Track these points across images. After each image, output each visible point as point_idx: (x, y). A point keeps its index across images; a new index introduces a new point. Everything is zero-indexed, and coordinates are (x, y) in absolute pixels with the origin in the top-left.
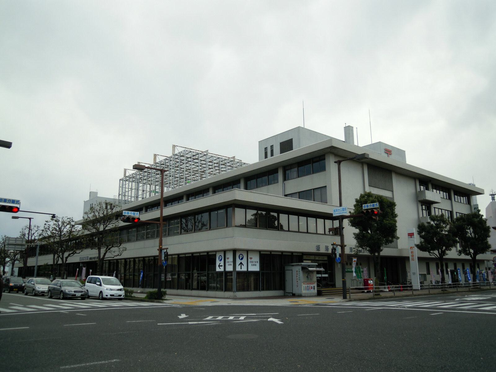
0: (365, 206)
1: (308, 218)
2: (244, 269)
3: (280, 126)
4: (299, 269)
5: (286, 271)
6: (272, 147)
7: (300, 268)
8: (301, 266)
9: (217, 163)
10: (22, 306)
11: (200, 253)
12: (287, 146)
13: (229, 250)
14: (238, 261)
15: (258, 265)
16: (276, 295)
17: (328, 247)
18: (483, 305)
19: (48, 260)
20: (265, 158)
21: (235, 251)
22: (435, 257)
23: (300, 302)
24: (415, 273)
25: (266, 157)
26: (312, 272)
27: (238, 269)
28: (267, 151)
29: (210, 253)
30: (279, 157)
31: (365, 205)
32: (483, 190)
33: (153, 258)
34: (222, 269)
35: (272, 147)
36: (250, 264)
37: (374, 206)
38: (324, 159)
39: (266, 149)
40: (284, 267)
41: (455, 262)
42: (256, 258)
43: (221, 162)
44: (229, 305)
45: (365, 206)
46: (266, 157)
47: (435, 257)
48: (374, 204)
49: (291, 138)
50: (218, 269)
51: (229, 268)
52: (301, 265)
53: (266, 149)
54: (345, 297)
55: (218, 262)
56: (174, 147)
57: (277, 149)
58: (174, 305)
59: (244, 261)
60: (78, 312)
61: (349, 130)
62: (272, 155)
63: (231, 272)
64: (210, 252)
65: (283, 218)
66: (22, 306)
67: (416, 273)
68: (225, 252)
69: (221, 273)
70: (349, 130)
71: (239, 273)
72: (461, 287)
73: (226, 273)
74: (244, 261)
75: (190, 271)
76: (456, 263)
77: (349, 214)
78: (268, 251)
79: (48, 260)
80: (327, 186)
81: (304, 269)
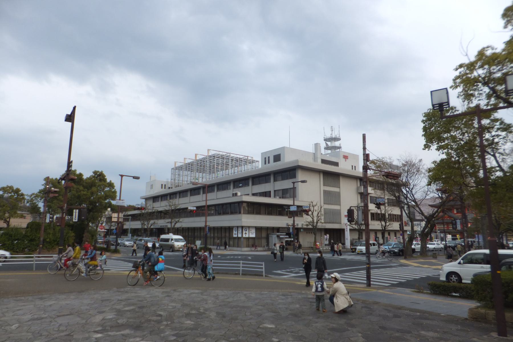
2: (247, 236)
6: (269, 157)
10: (508, 260)
12: (277, 158)
13: (240, 226)
14: (244, 232)
15: (254, 234)
19: (137, 225)
21: (242, 227)
25: (265, 164)
26: (282, 238)
27: (244, 236)
28: (266, 160)
34: (236, 236)
35: (269, 157)
36: (250, 234)
39: (265, 158)
42: (254, 231)
43: (239, 161)
46: (265, 164)
50: (234, 236)
51: (240, 236)
54: (294, 252)
55: (234, 232)
56: (209, 150)
57: (272, 159)
58: (63, 296)
59: (247, 232)
62: (269, 163)
63: (240, 238)
66: (508, 260)
68: (238, 227)
69: (235, 238)
71: (244, 238)
73: (239, 238)
74: (247, 232)
77: (498, 111)
79: (137, 225)
81: (278, 236)
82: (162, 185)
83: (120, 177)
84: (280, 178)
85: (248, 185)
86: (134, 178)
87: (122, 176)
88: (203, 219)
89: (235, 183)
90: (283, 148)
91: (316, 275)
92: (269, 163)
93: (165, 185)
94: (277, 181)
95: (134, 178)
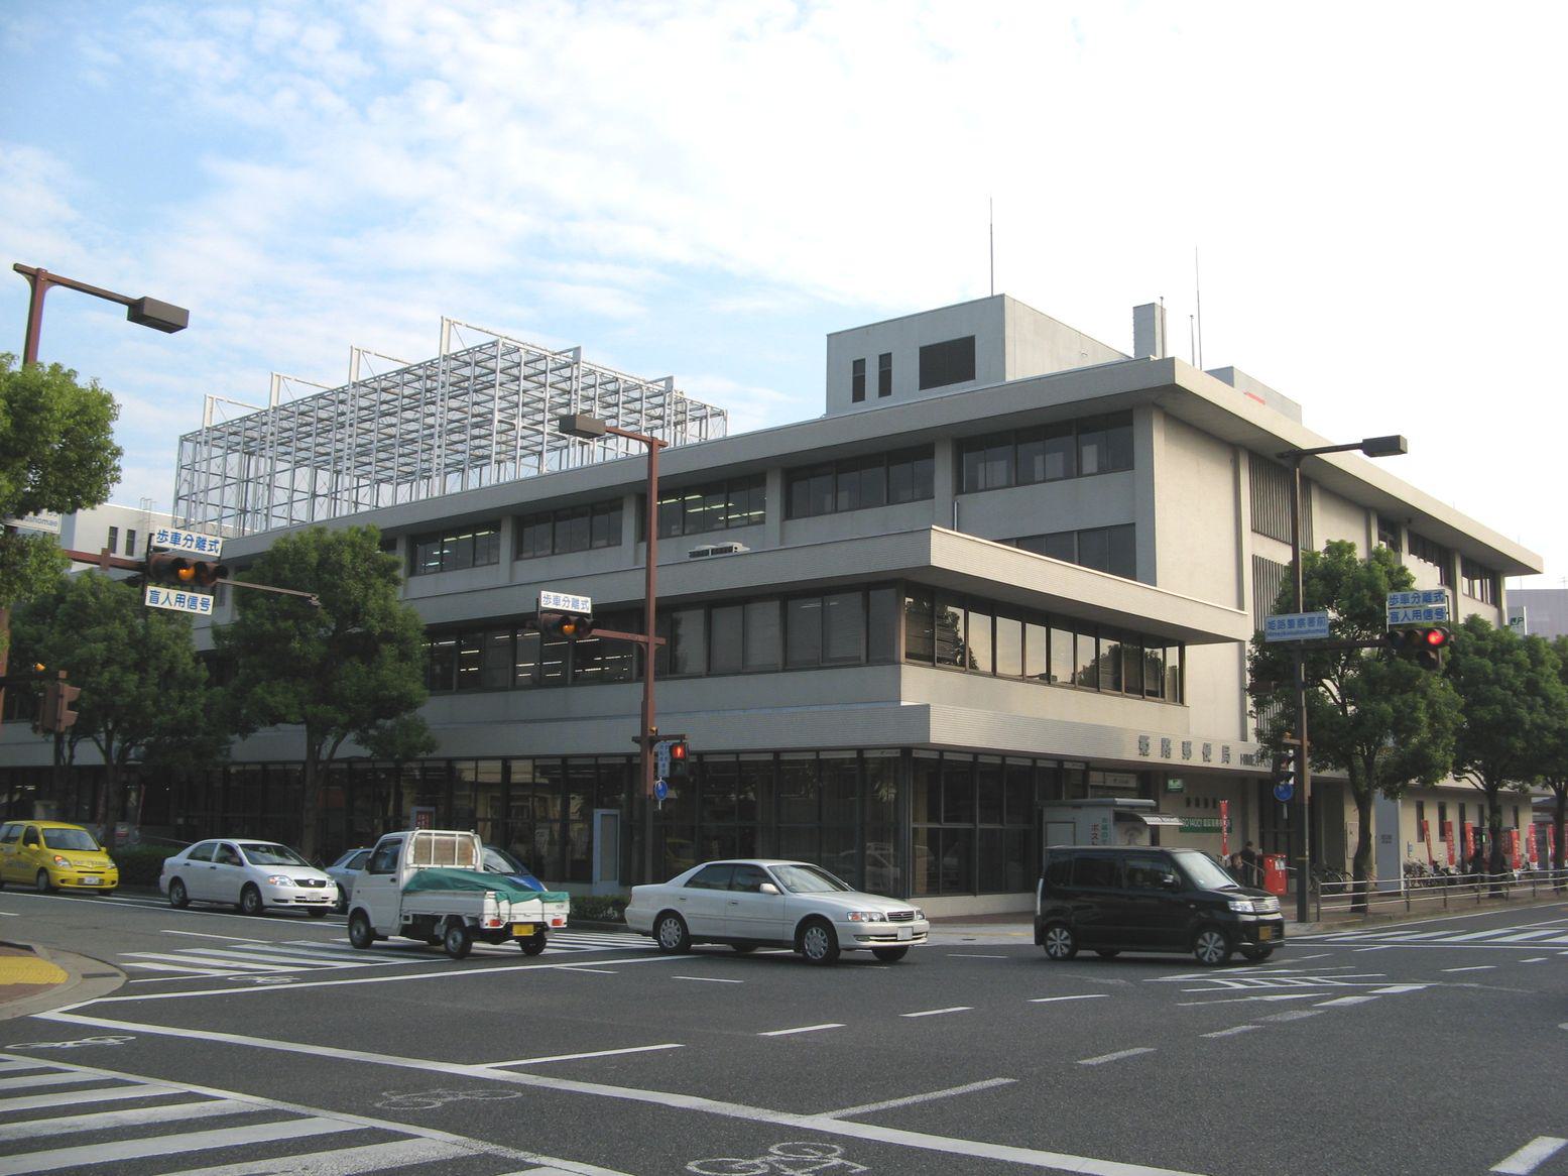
0: (548, 598)
1: (1053, 631)
3: (915, 285)
4: (1104, 820)
5: (1049, 825)
6: (885, 360)
7: (1109, 814)
8: (1112, 809)
9: (458, 409)
11: (737, 753)
16: (1011, 909)
17: (1169, 742)
18: (995, 942)
20: (855, 400)
22: (1474, 787)
23: (390, 937)
24: (1390, 837)
25: (859, 394)
29: (785, 757)
30: (913, 407)
31: (549, 593)
32: (1540, 560)
33: (345, 766)
35: (885, 360)
37: (556, 598)
38: (1130, 423)
39: (859, 366)
40: (1042, 811)
41: (1480, 803)
44: (966, 943)
45: (548, 598)
46: (859, 394)
47: (1474, 787)
48: (195, 599)
49: (965, 334)
52: (1115, 805)
53: (859, 366)
57: (906, 371)
60: (1349, 972)
61: (1146, 319)
62: (885, 389)
64: (981, 754)
65: (977, 630)
67: (1394, 837)
70: (1146, 319)
72: (1514, 885)
75: (1220, 818)
76: (1444, 803)
78: (967, 753)
80: (1137, 525)
82: (114, 531)
83: (24, 283)
84: (1000, 469)
85: (614, 539)
86: (140, 312)
87: (39, 281)
88: (628, 695)
89: (528, 531)
90: (993, 307)
91: (548, 944)
92: (885, 389)
93: (131, 534)
94: (974, 489)
95: (140, 312)
